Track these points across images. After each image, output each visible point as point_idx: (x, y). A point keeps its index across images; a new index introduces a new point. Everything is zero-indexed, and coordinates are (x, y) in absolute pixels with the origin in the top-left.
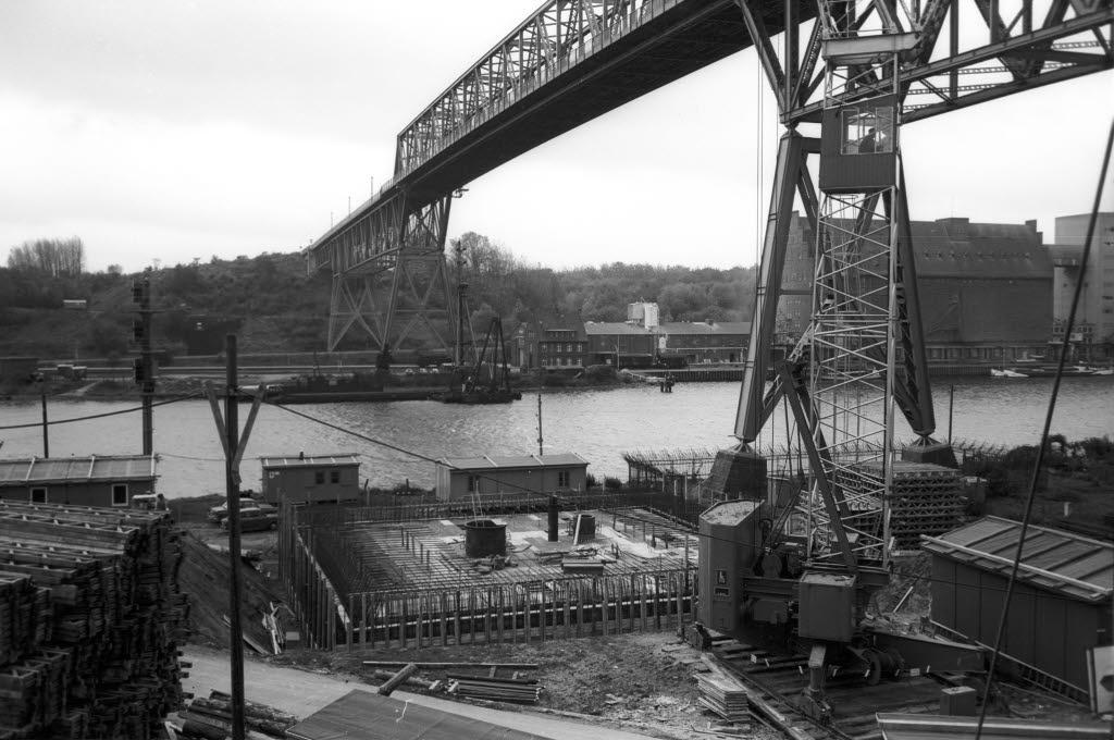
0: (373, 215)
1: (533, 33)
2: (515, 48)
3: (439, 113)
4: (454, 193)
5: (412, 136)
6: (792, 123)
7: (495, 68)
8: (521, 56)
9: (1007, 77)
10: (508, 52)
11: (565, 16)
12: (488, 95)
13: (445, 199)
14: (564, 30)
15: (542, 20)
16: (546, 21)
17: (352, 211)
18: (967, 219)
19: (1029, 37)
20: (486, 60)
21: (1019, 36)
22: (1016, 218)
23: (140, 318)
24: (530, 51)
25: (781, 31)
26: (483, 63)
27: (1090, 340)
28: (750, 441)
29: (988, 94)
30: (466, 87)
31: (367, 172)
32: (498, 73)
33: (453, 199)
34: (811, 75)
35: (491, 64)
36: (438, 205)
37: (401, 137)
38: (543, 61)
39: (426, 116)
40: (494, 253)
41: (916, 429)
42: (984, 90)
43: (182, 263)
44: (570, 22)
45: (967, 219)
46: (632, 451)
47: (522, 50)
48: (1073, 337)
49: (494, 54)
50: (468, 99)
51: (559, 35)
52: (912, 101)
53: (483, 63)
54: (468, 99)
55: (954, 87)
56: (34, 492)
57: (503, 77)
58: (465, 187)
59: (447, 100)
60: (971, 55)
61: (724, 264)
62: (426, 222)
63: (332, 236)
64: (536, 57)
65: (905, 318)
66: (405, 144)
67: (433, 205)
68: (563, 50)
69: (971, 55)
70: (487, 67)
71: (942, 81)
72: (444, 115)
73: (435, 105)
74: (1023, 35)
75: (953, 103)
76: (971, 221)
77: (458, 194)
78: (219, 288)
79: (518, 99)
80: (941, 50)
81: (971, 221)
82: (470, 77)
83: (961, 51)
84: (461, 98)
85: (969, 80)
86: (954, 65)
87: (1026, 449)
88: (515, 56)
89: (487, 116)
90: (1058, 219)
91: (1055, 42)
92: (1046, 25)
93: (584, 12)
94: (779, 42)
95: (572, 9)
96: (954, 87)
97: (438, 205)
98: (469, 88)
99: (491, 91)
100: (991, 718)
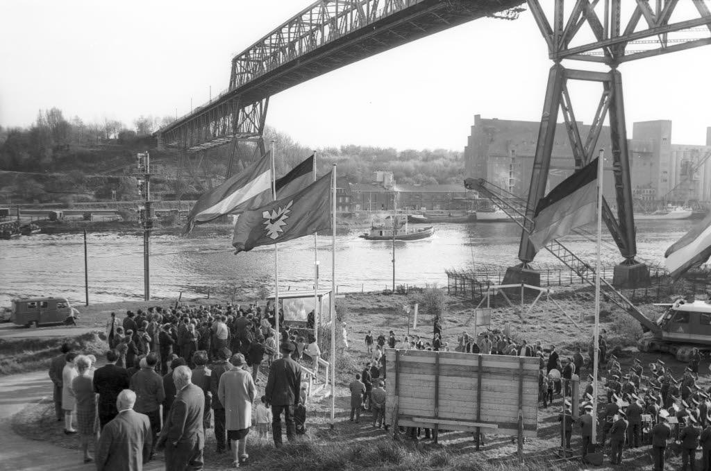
0: (211, 111)
5: (244, 60)
7: (273, 41)
13: (264, 101)
14: (292, 35)
18: (472, 127)
22: (470, 129)
25: (250, 104)
28: (529, 262)
31: (216, 84)
35: (271, 39)
36: (258, 106)
37: (235, 60)
41: (624, 255)
43: (68, 116)
46: (450, 268)
48: (498, 175)
51: (289, 38)
61: (702, 145)
65: (620, 185)
66: (238, 65)
67: (255, 106)
68: (292, 45)
70: (287, 29)
76: (584, 124)
79: (269, 71)
81: (584, 124)
83: (586, 23)
87: (635, 252)
90: (669, 122)
97: (258, 106)
98: (293, 30)
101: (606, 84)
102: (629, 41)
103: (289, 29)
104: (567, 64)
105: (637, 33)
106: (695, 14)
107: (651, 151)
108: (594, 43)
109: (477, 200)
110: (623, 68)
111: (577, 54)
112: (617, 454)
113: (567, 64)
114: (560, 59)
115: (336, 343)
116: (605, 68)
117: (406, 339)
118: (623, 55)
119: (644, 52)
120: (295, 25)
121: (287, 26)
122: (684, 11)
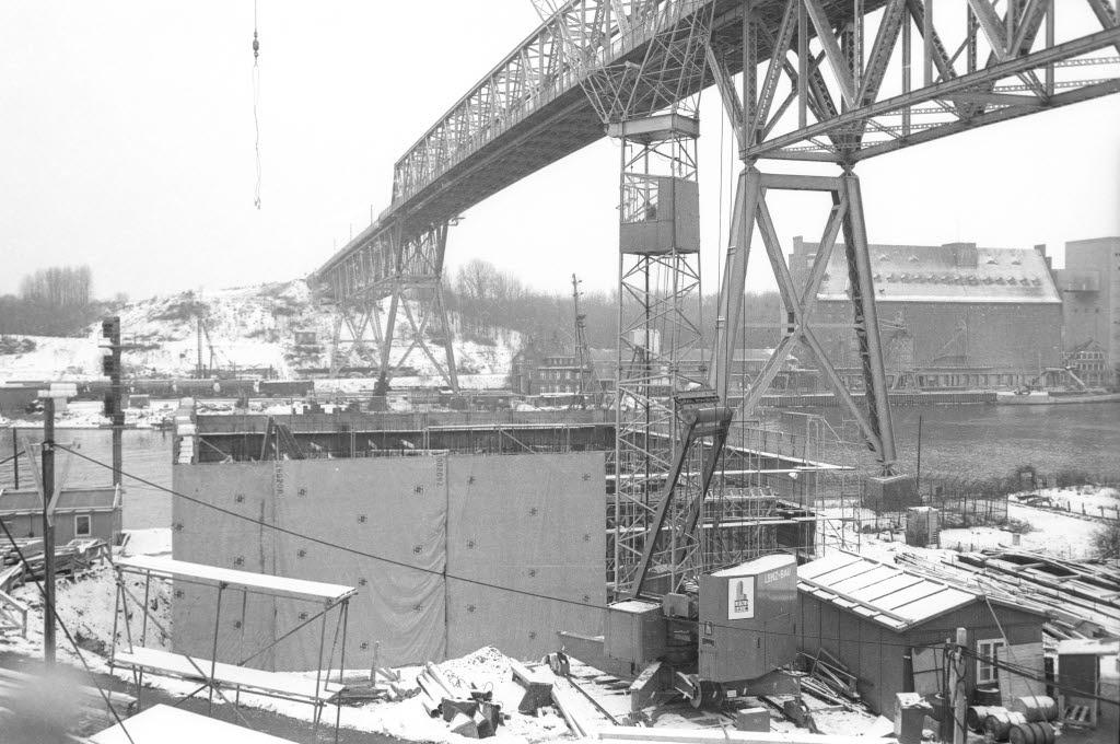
1: (518, 65)
2: (503, 80)
3: (474, 106)
4: (450, 221)
6: (749, 158)
7: (484, 98)
8: (542, 62)
9: (951, 118)
10: (496, 84)
11: (547, 49)
12: (504, 106)
15: (526, 54)
16: (531, 53)
17: (354, 237)
18: (974, 244)
19: (907, 97)
20: (476, 91)
21: (1042, 52)
23: (110, 353)
24: (516, 82)
25: (739, 72)
26: (473, 94)
27: (1101, 367)
29: (874, 151)
30: (543, 44)
31: (368, 199)
32: (486, 103)
33: (449, 227)
34: (768, 111)
35: (480, 95)
37: (398, 166)
38: (567, 67)
39: (421, 145)
40: (500, 279)
42: (931, 129)
44: (596, 23)
45: (974, 244)
47: (509, 81)
49: (483, 85)
50: (511, 88)
52: (869, 138)
53: (473, 94)
54: (511, 88)
55: (906, 125)
56: (78, 519)
57: (489, 108)
58: (461, 215)
59: (440, 130)
60: (1089, 41)
62: (424, 248)
63: (334, 264)
64: (558, 63)
69: (1089, 41)
70: (537, 48)
71: (894, 120)
72: (480, 109)
73: (429, 135)
74: (969, 74)
75: (905, 141)
77: (455, 222)
78: (831, 337)
80: (1039, 44)
82: (461, 107)
84: (453, 127)
85: (1068, 75)
86: (904, 103)
88: (502, 88)
89: (504, 127)
90: (1068, 244)
91: (999, 83)
92: (989, 66)
93: (612, 13)
94: (738, 80)
95: (553, 43)
96: (906, 125)
98: (460, 118)
99: (508, 102)
100: (784, 598)
101: (835, 194)
102: (1058, 60)
103: (542, 48)
104: (763, 165)
105: (1037, 53)
106: (1092, 25)
107: (1096, 288)
108: (1093, 36)
109: (795, 373)
110: (861, 169)
111: (775, 151)
112: (756, 721)
113: (764, 166)
114: (755, 158)
115: (260, 446)
116: (835, 170)
117: (484, 522)
118: (858, 149)
119: (1101, 84)
120: (551, 39)
121: (538, 41)
122: (1073, 17)
